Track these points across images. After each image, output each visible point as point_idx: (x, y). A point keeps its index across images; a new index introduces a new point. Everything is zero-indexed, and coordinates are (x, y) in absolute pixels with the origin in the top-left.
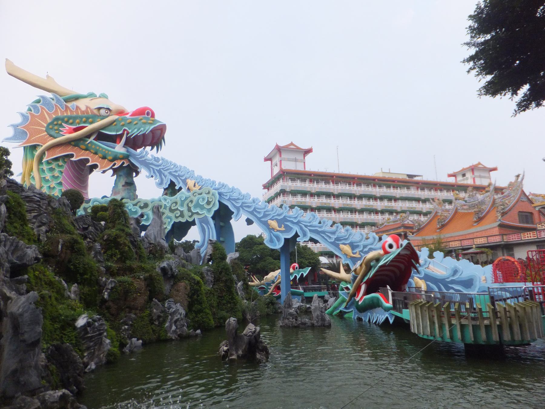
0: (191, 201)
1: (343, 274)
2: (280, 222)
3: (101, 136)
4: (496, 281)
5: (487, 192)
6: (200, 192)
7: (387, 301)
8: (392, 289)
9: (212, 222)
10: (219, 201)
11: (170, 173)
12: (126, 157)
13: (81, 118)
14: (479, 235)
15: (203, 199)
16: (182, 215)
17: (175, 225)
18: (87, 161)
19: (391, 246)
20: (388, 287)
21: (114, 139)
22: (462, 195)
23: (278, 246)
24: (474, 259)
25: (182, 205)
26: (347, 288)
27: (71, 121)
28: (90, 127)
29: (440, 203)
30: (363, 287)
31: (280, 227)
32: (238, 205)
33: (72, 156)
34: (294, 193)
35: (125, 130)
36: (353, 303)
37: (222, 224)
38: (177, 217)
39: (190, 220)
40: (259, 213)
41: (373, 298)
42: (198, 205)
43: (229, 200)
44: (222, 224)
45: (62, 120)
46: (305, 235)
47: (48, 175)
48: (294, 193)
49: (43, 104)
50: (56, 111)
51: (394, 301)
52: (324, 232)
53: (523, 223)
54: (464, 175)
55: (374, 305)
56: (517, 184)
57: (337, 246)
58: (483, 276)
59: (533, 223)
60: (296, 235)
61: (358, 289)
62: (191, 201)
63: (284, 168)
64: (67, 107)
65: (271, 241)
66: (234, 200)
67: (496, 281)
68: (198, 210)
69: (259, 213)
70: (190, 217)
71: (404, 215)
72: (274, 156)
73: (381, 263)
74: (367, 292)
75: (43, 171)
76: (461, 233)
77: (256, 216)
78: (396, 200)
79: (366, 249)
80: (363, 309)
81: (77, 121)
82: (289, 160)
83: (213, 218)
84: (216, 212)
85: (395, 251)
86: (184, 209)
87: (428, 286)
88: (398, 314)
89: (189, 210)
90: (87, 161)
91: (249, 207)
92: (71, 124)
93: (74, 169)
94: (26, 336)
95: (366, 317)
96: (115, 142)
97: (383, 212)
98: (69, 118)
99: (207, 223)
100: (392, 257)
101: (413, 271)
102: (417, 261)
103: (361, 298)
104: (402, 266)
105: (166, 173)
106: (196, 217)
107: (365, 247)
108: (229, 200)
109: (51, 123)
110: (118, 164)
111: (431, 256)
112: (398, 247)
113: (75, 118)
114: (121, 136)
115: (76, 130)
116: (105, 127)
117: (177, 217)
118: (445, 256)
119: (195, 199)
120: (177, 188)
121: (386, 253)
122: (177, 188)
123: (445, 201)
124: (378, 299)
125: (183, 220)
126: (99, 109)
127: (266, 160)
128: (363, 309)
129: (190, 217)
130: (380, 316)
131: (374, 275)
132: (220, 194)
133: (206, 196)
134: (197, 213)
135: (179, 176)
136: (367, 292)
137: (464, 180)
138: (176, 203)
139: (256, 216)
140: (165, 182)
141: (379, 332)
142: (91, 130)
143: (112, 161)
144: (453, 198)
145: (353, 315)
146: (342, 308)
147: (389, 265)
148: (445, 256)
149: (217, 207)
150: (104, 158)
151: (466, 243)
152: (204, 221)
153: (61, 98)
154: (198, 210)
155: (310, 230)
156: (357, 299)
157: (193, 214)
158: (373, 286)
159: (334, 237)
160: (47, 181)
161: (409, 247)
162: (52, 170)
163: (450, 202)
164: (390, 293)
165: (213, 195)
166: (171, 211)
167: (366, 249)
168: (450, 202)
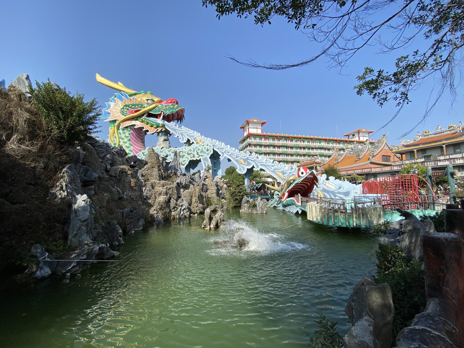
0: (199, 149)
1: (276, 187)
2: (245, 160)
3: (150, 115)
4: (363, 193)
5: (365, 144)
6: (203, 144)
7: (298, 202)
8: (302, 195)
9: (209, 160)
10: (213, 150)
11: (187, 135)
12: (163, 126)
13: (138, 105)
14: (358, 168)
15: (205, 148)
16: (194, 157)
17: (191, 162)
18: (143, 128)
19: (302, 173)
20: (299, 194)
21: (156, 116)
22: (350, 146)
23: (244, 172)
24: (353, 180)
25: (194, 151)
26: (278, 195)
27: (133, 107)
28: (143, 110)
29: (337, 151)
30: (287, 194)
31: (245, 163)
32: (223, 151)
33: (135, 125)
34: (255, 145)
35: (162, 111)
36: (280, 202)
37: (215, 161)
38: (191, 158)
39: (198, 159)
40: (234, 155)
41: (291, 200)
42: (202, 151)
43: (218, 149)
44: (215, 161)
45: (129, 106)
46: (258, 167)
47: (123, 136)
48: (255, 145)
49: (118, 98)
50: (125, 101)
51: (302, 202)
52: (268, 166)
53: (384, 162)
54: (354, 135)
55: (292, 204)
56: (262, 18)
57: (275, 173)
58: (356, 190)
59: (390, 162)
60: (253, 167)
61: (284, 195)
62: (199, 149)
63: (250, 132)
64: (130, 99)
65: (240, 170)
66: (221, 149)
67: (363, 193)
68: (202, 154)
69: (234, 155)
70: (198, 157)
71: (316, 157)
72: (246, 125)
73: (296, 182)
74: (289, 196)
75: (120, 134)
76: (348, 167)
77: (232, 157)
78: (313, 148)
79: (291, 175)
80: (285, 206)
81: (137, 107)
82: (253, 128)
83: (210, 158)
84: (211, 155)
85: (304, 176)
86: (195, 153)
87: (324, 195)
88: (304, 209)
89: (198, 154)
90: (143, 128)
91: (229, 152)
92: (133, 108)
93: (137, 132)
94: (80, 217)
95: (287, 209)
96: (157, 118)
97: (304, 155)
98: (132, 105)
99: (207, 161)
100: (302, 179)
101: (315, 186)
102: (317, 181)
103: (285, 200)
104: (309, 184)
105: (185, 134)
106: (201, 157)
107: (290, 173)
108: (218, 149)
109: (123, 108)
110: (159, 129)
111: (327, 179)
112: (306, 174)
113: (135, 105)
114: (160, 115)
115: (136, 111)
116: (151, 110)
117: (191, 158)
118: (336, 179)
119: (200, 148)
120: (191, 142)
121: (299, 176)
122: (191, 142)
123: (340, 150)
124: (294, 201)
125: (195, 159)
126: (148, 100)
127: (241, 128)
128: (285, 206)
129: (198, 157)
130: (294, 210)
131: (292, 188)
132: (213, 146)
133: (206, 147)
134: (202, 156)
135: (192, 136)
136: (289, 196)
137: (353, 138)
138: (191, 150)
139: (232, 157)
140: (185, 139)
141: (294, 218)
142: (144, 112)
143: (156, 128)
144: (345, 148)
145: (280, 207)
146: (275, 205)
147: (300, 183)
148: (336, 179)
149: (212, 152)
150: (152, 126)
151: (350, 172)
152: (205, 159)
153: (127, 95)
154: (202, 154)
155: (261, 165)
156: (283, 200)
157: (200, 156)
158: (292, 194)
159: (273, 168)
160: (123, 139)
161: (312, 174)
162: (124, 133)
163: (343, 150)
164: (300, 197)
165: (210, 146)
166: (188, 154)
167: (291, 175)
168: (343, 150)
